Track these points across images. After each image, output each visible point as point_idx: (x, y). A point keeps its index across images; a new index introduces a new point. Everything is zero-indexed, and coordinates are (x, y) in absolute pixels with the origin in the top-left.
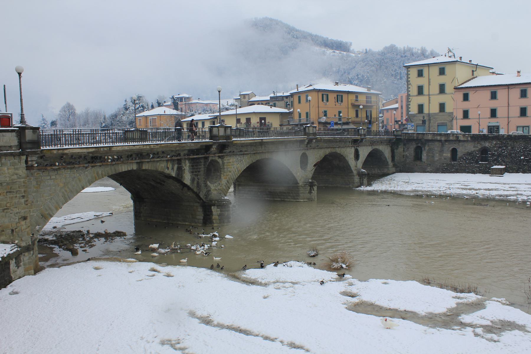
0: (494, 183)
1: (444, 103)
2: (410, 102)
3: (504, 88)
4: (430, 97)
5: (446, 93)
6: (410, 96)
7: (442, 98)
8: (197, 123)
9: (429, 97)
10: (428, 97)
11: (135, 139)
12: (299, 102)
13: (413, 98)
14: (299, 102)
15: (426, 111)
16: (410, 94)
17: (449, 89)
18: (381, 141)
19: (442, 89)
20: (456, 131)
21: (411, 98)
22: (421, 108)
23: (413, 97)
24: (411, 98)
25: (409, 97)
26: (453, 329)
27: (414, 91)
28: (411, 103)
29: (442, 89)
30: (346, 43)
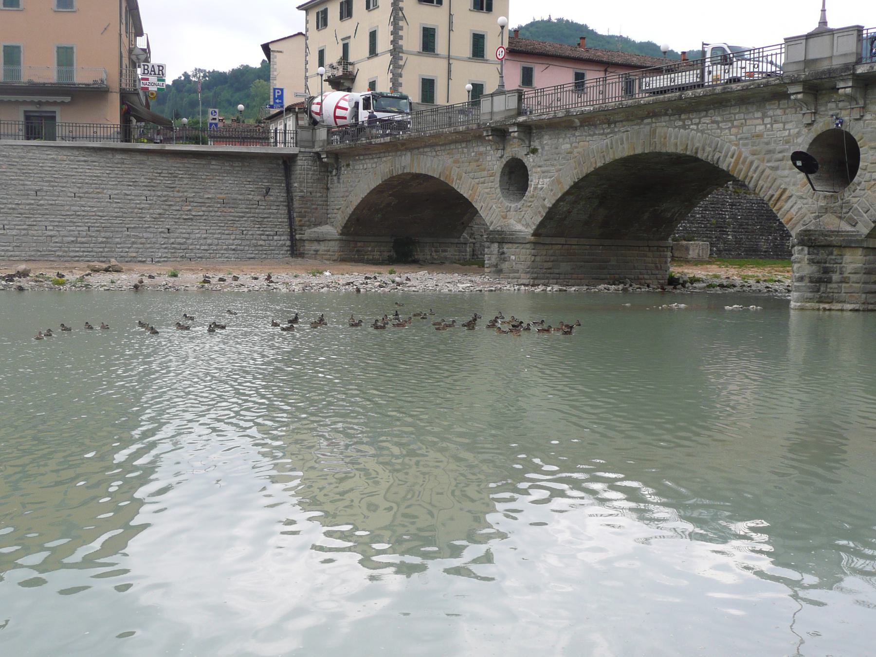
0: (454, 616)
1: (482, 85)
2: (401, 67)
3: (597, 69)
4: (451, 62)
5: (487, 60)
6: (402, 52)
7: (432, 67)
8: (791, 267)
9: (449, 64)
10: (445, 62)
11: (76, 138)
12: (373, 35)
13: (411, 57)
14: (373, 35)
15: (440, 99)
16: (401, 47)
17: (494, 47)
18: (355, 187)
19: (478, 43)
20: (642, 290)
21: (404, 56)
22: (428, 86)
23: (409, 56)
24: (404, 56)
25: (401, 55)
26: (155, 143)
27: (412, 40)
28: (404, 72)
29: (478, 43)
30: (95, 82)
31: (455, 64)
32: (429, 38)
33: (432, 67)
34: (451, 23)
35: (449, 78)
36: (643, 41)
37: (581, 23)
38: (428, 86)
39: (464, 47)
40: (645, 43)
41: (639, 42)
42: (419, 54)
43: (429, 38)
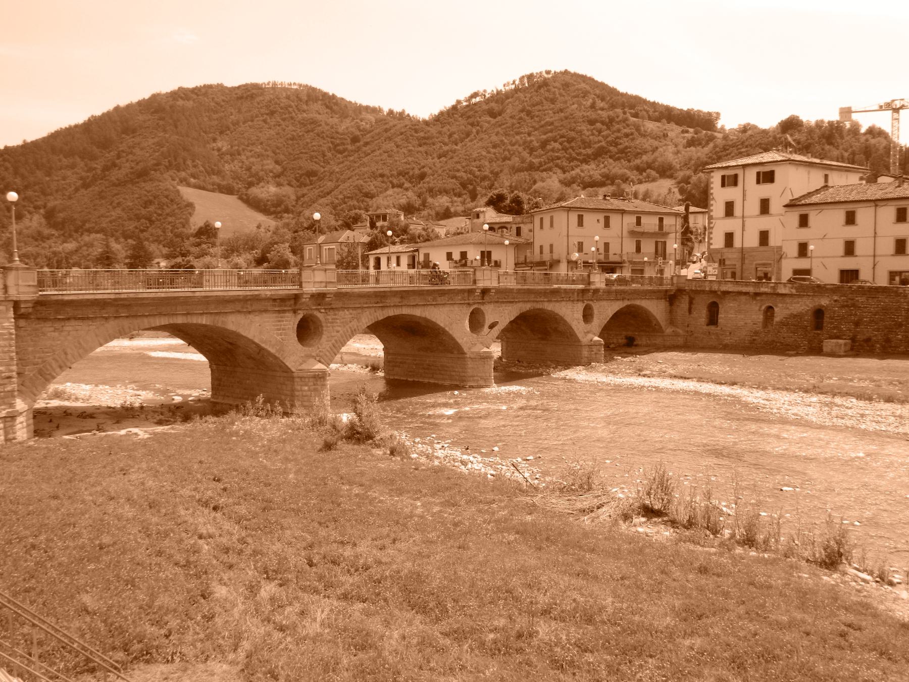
7: (732, 225)
12: (542, 227)
13: (718, 222)
14: (542, 227)
15: (737, 243)
17: (776, 206)
19: (765, 206)
22: (729, 237)
29: (765, 206)
31: (748, 221)
32: (729, 209)
33: (732, 225)
34: (744, 195)
35: (743, 230)
36: (30, 139)
37: (147, 96)
38: (729, 237)
39: (756, 208)
40: (107, 117)
41: (137, 101)
42: (723, 218)
43: (729, 209)
